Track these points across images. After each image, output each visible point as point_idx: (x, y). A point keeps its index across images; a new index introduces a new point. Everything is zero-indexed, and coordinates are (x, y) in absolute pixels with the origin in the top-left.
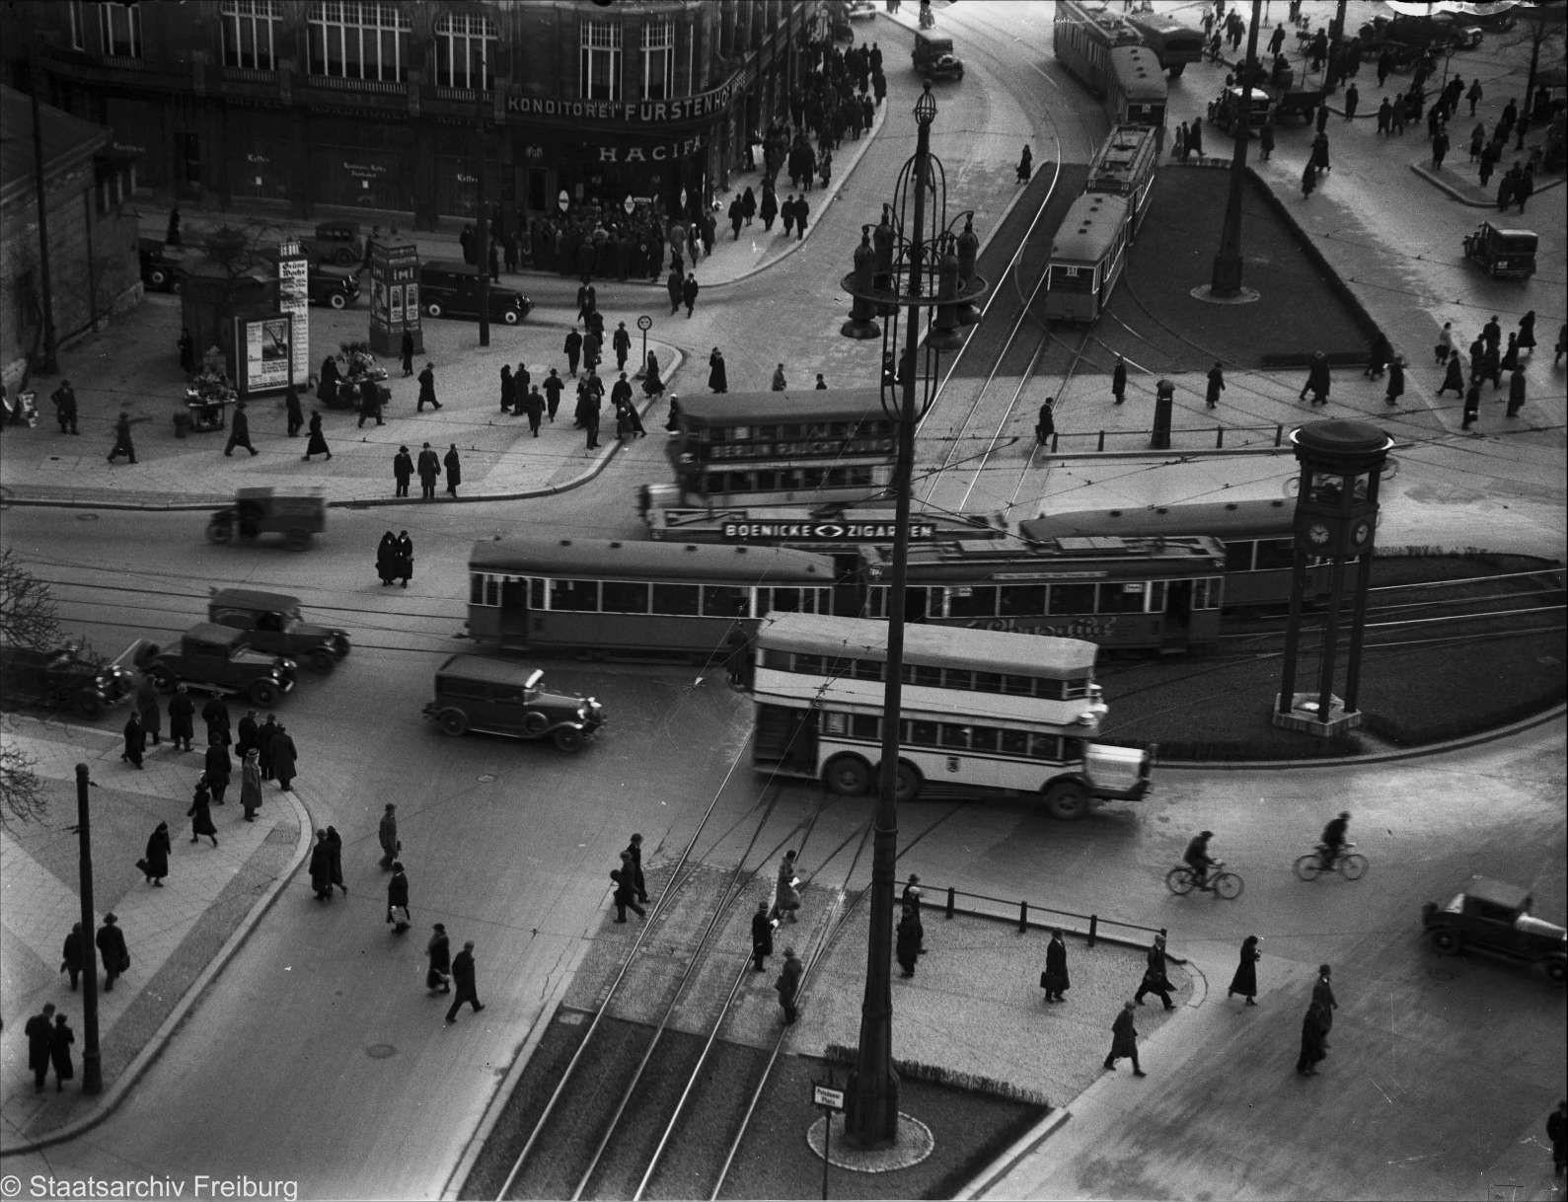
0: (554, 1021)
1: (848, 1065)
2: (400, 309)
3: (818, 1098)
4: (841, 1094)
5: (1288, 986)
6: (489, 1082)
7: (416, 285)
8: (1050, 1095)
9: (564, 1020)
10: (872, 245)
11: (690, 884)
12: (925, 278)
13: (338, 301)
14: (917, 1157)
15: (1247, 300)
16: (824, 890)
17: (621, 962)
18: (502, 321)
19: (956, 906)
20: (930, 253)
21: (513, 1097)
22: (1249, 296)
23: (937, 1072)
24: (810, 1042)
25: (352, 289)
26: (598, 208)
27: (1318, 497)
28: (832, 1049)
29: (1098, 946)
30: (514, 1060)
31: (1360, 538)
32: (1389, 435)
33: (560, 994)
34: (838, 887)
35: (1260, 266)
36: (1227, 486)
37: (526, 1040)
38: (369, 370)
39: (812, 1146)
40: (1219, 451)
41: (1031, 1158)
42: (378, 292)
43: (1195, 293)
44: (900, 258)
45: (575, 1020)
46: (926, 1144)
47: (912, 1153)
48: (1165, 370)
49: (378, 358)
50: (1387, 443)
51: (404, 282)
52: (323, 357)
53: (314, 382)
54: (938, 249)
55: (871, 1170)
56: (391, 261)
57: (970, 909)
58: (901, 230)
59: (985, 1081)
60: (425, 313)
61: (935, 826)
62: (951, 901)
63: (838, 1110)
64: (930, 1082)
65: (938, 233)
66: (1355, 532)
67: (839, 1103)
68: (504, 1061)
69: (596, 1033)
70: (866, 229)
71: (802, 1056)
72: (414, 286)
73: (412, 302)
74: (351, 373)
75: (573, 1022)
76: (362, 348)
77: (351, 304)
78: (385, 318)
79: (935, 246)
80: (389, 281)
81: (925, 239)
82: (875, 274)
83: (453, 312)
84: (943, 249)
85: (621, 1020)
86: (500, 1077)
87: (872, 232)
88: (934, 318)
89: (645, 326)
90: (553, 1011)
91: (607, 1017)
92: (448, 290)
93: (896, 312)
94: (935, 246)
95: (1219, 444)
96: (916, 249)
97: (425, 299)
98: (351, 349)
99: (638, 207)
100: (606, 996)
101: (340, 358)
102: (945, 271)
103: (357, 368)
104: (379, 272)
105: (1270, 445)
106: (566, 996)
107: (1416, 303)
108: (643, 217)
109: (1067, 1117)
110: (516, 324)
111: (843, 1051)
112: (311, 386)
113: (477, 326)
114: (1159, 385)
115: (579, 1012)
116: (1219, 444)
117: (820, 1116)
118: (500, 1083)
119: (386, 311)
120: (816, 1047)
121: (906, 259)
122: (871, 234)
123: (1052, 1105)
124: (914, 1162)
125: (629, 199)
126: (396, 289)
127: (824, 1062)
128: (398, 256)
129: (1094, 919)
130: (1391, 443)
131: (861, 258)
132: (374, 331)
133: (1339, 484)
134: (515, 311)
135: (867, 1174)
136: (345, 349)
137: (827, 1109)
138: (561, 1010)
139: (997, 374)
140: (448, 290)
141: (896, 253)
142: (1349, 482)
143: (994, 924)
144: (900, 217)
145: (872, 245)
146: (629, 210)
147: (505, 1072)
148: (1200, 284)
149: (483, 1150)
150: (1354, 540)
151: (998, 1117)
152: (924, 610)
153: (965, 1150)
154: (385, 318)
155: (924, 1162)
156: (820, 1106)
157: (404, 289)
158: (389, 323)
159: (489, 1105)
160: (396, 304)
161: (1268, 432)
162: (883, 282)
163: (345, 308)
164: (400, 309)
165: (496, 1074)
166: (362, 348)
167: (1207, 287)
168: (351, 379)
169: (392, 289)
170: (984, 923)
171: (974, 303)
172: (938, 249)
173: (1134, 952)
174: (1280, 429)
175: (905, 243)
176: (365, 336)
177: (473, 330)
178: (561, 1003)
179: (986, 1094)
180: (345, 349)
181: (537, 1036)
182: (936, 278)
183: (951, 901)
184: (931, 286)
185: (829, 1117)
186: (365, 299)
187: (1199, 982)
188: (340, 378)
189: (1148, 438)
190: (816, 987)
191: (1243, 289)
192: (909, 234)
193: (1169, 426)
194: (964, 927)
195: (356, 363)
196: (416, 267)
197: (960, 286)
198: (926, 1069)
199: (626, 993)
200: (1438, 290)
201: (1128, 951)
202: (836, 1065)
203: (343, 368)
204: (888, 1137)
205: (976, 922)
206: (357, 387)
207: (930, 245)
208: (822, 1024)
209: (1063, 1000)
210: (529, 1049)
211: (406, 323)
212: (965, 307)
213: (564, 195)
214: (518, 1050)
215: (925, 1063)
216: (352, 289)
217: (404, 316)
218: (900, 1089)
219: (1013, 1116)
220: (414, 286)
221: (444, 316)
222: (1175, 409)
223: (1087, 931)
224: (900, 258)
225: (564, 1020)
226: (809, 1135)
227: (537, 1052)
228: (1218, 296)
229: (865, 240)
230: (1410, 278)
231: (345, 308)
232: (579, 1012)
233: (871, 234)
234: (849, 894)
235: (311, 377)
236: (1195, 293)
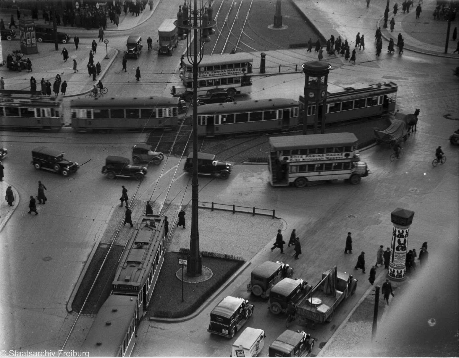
0: (98, 248)
1: (186, 254)
2: (30, 40)
3: (180, 262)
4: (186, 261)
5: (309, 223)
6: (82, 265)
7: (34, 32)
8: (245, 258)
9: (101, 246)
10: (182, 11)
11: (136, 206)
12: (198, 21)
13: (9, 38)
14: (208, 278)
15: (284, 28)
16: (175, 205)
17: (117, 229)
18: (62, 43)
19: (255, 212)
20: (199, 14)
21: (88, 269)
22: (284, 27)
23: (212, 254)
24: (175, 248)
25: (13, 34)
26: (88, 7)
27: (311, 84)
28: (181, 249)
29: (256, 216)
30: (88, 259)
31: (323, 95)
32: (329, 65)
33: (99, 240)
34: (179, 204)
35: (287, 18)
36: (284, 82)
37: (91, 253)
38: (22, 59)
39: (178, 277)
40: (280, 73)
41: (240, 276)
42: (22, 35)
43: (269, 27)
44: (191, 15)
45: (105, 246)
46: (210, 274)
47: (206, 277)
48: (263, 51)
49: (25, 55)
50: (329, 67)
51: (30, 31)
52: (7, 55)
53: (4, 63)
54: (202, 12)
55: (195, 282)
56: (26, 25)
57: (218, 208)
58: (190, 7)
59: (226, 256)
60: (37, 41)
61: (207, 184)
62: (254, 211)
63: (185, 265)
64: (210, 257)
65: (201, 7)
66: (321, 94)
67: (186, 263)
68: (85, 260)
69: (111, 250)
70: (180, 7)
71: (173, 252)
72: (34, 32)
73: (33, 37)
74: (17, 60)
75: (104, 247)
76: (19, 52)
77: (14, 39)
78: (25, 43)
79: (201, 11)
80: (26, 30)
81: (197, 9)
82: (183, 20)
83: (46, 40)
84: (203, 12)
85: (119, 246)
86: (84, 264)
87: (182, 7)
88: (202, 33)
89: (107, 42)
90: (98, 244)
91: (114, 245)
92: (44, 34)
93: (190, 31)
94: (201, 11)
95: (279, 71)
96: (195, 13)
97: (37, 37)
98: (16, 52)
99: (100, 6)
100: (113, 239)
101: (13, 55)
102: (204, 18)
103: (19, 58)
104: (22, 28)
105: (294, 71)
106: (102, 240)
107: (332, 27)
108: (102, 9)
109: (250, 264)
110: (66, 43)
111: (185, 250)
112: (4, 64)
113: (54, 44)
114: (261, 54)
115: (106, 244)
116: (279, 71)
117: (180, 268)
118: (84, 266)
119: (26, 40)
120: (177, 250)
121: (192, 16)
122: (181, 8)
123: (245, 261)
124: (207, 279)
125: (97, 4)
126: (28, 33)
127: (179, 253)
128: (28, 23)
129: (254, 208)
130: (330, 67)
131: (179, 16)
132: (22, 47)
133: (316, 80)
134: (65, 39)
135: (194, 284)
136: (14, 52)
137: (183, 265)
138: (100, 244)
139: (213, 53)
140: (44, 34)
141: (189, 13)
142: (319, 80)
143: (225, 212)
144: (190, 3)
145: (182, 11)
146: (98, 7)
147: (86, 262)
148: (270, 24)
149: (81, 285)
150: (321, 96)
151: (231, 265)
152: (213, 123)
153: (221, 275)
154: (25, 43)
155: (210, 279)
156: (180, 265)
157: (31, 33)
158: (27, 44)
159: (81, 272)
160: (28, 38)
161: (293, 67)
162: (186, 23)
163: (12, 40)
164: (30, 40)
165: (83, 263)
166: (19, 52)
167: (272, 25)
168: (17, 61)
169: (27, 33)
170: (222, 212)
171: (213, 28)
172: (202, 12)
173: (266, 217)
174: (297, 66)
175: (192, 11)
176: (19, 48)
177: (53, 46)
178: (100, 242)
179: (227, 259)
180: (14, 52)
181: (94, 252)
182: (202, 21)
183: (254, 211)
184: (200, 23)
185: (183, 268)
186: (18, 37)
187: (285, 224)
188: (13, 61)
189: (259, 70)
190: (175, 233)
191: (283, 25)
192: (193, 8)
193: (265, 66)
194: (217, 213)
195: (18, 56)
196: (34, 26)
197: (209, 23)
198: (209, 253)
199: (120, 238)
200: (338, 23)
201: (264, 217)
202: (183, 253)
203: (14, 59)
204: (200, 272)
205: (220, 211)
206: (19, 64)
207: (199, 11)
208: (178, 243)
209: (352, 253)
210: (92, 256)
211: (32, 44)
212: (210, 29)
213: (77, 3)
214: (89, 256)
215: (209, 252)
216: (13, 34)
217: (31, 42)
218: (202, 259)
219: (235, 264)
220: (34, 32)
221: (43, 42)
222: (266, 61)
223: (252, 212)
224: (191, 15)
225: (101, 246)
226: (177, 274)
227: (94, 256)
228: (275, 27)
229: (180, 10)
230: (330, 20)
231: (12, 40)
232: (106, 244)
233: (181, 8)
234: (182, 206)
235: (3, 61)
236: (269, 27)
